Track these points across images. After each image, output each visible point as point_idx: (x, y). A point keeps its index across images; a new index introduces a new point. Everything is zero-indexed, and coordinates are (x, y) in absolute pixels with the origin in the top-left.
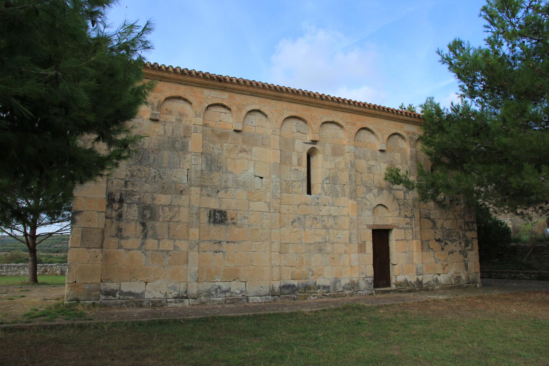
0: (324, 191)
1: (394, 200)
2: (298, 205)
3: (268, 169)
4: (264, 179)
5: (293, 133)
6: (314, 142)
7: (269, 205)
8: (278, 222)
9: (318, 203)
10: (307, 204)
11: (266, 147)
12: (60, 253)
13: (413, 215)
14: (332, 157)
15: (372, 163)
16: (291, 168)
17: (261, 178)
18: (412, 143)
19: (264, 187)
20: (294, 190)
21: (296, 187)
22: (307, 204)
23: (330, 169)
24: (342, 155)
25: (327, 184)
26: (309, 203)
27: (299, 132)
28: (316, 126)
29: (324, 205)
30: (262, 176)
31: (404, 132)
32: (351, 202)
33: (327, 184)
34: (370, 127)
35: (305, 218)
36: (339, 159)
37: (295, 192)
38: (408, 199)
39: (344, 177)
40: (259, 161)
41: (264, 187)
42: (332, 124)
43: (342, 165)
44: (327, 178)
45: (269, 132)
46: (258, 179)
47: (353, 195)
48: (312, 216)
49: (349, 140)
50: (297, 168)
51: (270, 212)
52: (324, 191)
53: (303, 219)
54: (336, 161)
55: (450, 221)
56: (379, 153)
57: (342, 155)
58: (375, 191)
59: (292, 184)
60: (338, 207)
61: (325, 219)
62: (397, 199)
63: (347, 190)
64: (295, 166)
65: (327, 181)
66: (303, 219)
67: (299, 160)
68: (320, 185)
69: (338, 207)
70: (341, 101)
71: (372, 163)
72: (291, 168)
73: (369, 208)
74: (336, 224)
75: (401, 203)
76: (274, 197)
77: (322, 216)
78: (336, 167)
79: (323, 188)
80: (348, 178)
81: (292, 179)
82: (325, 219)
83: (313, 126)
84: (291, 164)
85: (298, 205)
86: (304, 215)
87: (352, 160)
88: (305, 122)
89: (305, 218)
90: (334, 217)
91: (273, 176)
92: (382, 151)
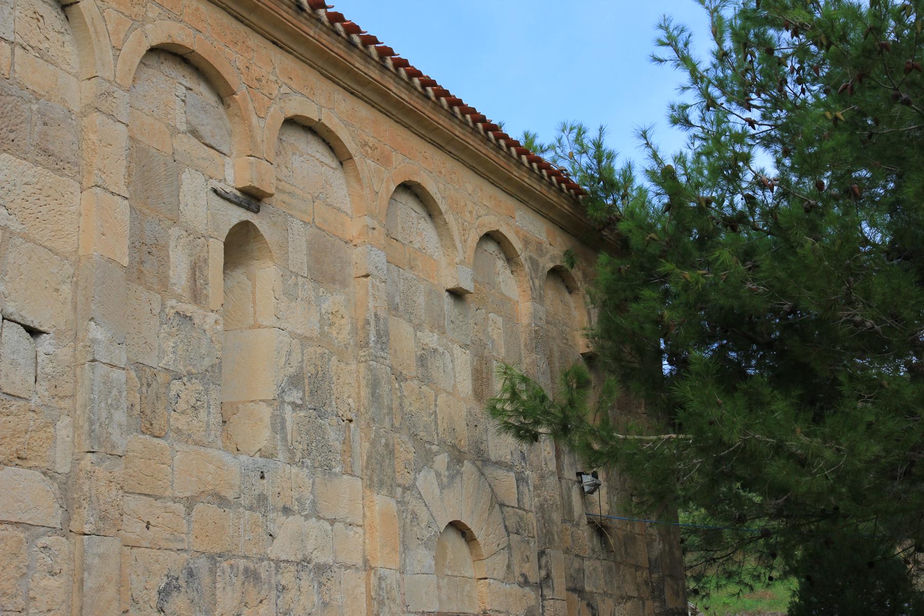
0: (284, 439)
1: (492, 507)
2: (190, 503)
3: (66, 289)
4: (45, 344)
5: (174, 131)
6: (252, 198)
7: (68, 492)
8: (111, 592)
9: (262, 498)
10: (222, 501)
11: (60, 171)
12: (283, 421)
13: (548, 576)
14: (309, 285)
15: (431, 339)
16: (163, 306)
17: (34, 332)
18: (537, 282)
19: (43, 388)
20: (180, 421)
21: (182, 405)
22: (222, 501)
23: (305, 340)
24: (344, 284)
25: (295, 406)
26: (230, 495)
27: (194, 133)
28: (266, 126)
29: (286, 511)
30: (35, 325)
31: (517, 233)
32: (381, 502)
33: (295, 406)
34: (431, 187)
35: (212, 572)
36: (333, 301)
37: (178, 431)
38: (527, 507)
39: (349, 385)
40: (26, 238)
41: (43, 388)
42: (310, 137)
43: (342, 333)
44: (295, 381)
45: (78, 93)
46: (14, 333)
47: (380, 475)
48: (242, 563)
49: (368, 220)
50: (189, 308)
51: (65, 531)
52: (284, 439)
53: (206, 579)
54: (325, 306)
55: (629, 604)
56: (447, 299)
57: (344, 284)
58: (442, 460)
59: (168, 385)
60: (332, 522)
61: (287, 578)
62: (502, 505)
63: (362, 448)
64: (179, 298)
65: (295, 396)
66: (206, 579)
67: (196, 269)
68: (266, 412)
69: (332, 522)
70: (356, 39)
71: (431, 339)
72: (163, 306)
73: (426, 534)
74: (325, 605)
75: (512, 523)
76: (99, 446)
77: (278, 562)
78: (322, 333)
79: (278, 425)
80: (365, 392)
81: (168, 360)
82: (287, 578)
83: (254, 119)
84: (164, 283)
85: (190, 503)
86: (214, 558)
87: (382, 314)
88: (222, 91)
89: (212, 572)
90: (321, 569)
91: (97, 332)
92: (457, 294)
